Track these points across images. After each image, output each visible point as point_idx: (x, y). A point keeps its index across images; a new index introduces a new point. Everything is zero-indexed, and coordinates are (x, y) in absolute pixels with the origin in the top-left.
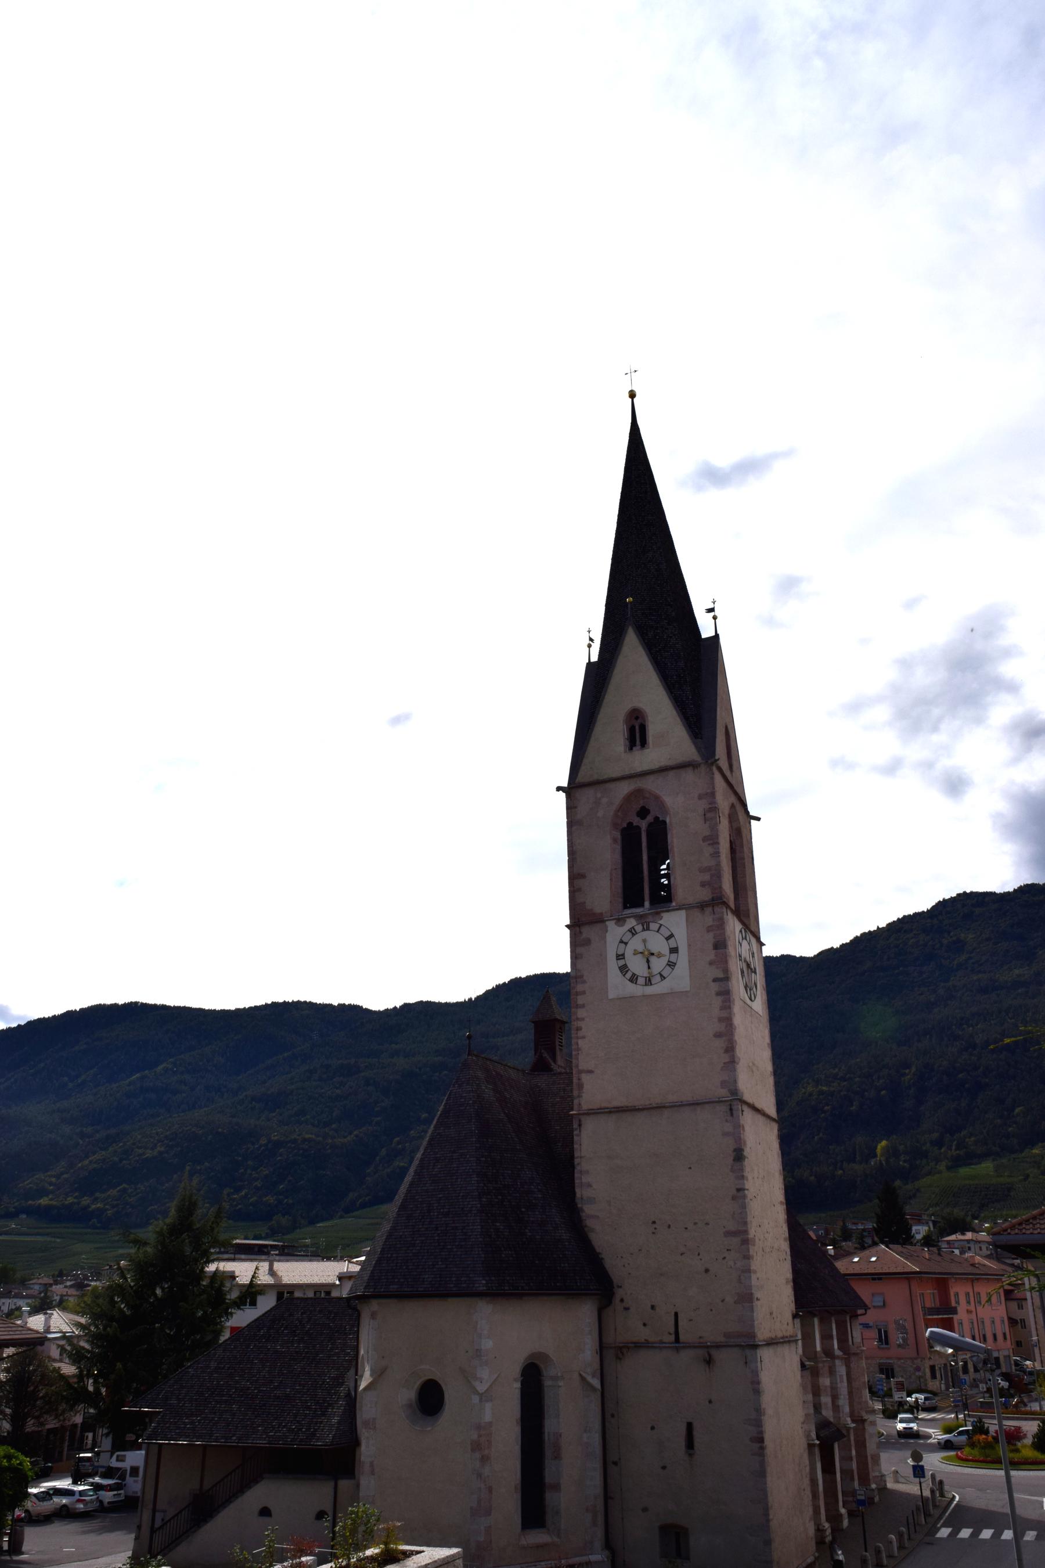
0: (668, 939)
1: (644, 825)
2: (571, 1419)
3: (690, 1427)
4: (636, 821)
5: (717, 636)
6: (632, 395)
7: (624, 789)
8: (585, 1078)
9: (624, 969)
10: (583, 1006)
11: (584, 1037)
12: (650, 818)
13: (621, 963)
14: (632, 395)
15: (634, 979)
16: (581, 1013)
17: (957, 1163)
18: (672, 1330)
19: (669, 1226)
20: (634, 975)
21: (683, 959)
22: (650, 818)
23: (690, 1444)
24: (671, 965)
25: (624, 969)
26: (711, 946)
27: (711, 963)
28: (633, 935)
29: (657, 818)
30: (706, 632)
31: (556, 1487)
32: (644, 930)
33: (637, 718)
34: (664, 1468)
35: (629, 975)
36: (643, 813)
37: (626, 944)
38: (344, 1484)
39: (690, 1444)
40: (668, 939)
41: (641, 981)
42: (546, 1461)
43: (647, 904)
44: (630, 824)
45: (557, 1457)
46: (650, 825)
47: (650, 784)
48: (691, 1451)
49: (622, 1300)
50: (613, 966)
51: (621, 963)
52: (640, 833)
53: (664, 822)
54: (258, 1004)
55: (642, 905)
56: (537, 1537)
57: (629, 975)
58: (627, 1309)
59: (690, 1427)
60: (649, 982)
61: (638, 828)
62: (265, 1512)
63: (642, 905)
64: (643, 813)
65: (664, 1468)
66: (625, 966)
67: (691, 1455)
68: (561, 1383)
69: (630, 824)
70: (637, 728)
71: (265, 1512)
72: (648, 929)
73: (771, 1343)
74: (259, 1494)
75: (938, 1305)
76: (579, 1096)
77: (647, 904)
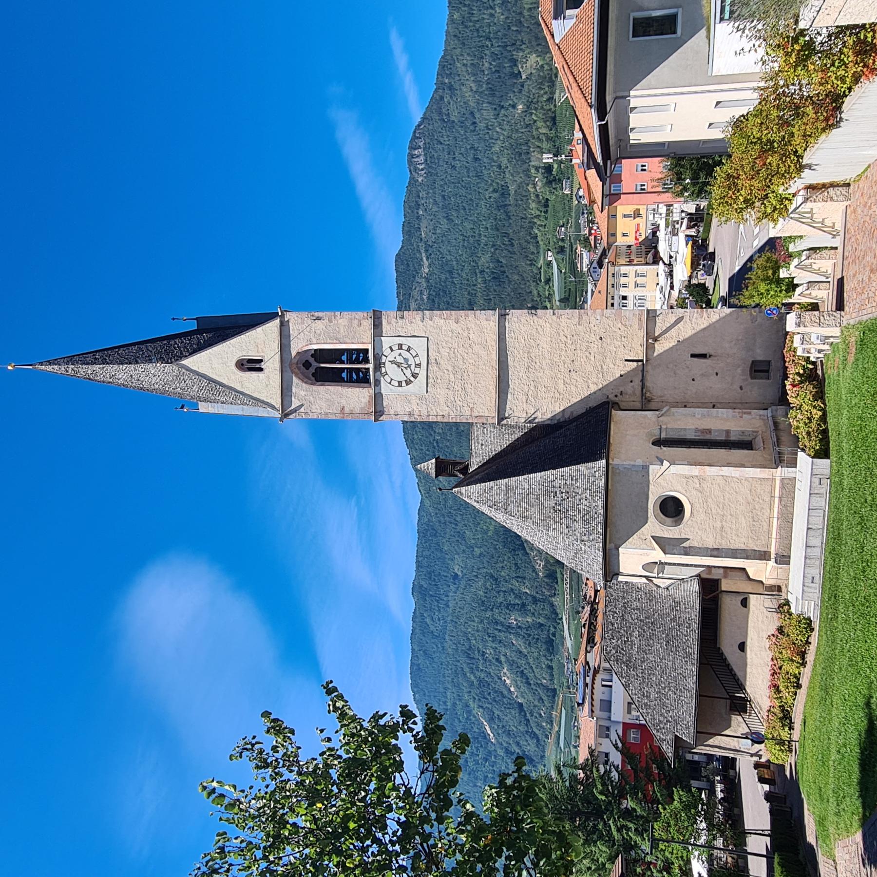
0: (392, 350)
1: (315, 364)
2: (688, 422)
3: (693, 356)
4: (312, 370)
12: (312, 360)
13: (404, 384)
17: (540, 281)
23: (703, 356)
25: (408, 382)
26: (400, 321)
29: (312, 356)
31: (728, 432)
34: (717, 374)
36: (307, 365)
38: (725, 585)
39: (703, 356)
40: (392, 350)
43: (367, 366)
44: (313, 375)
45: (709, 431)
49: (616, 396)
50: (405, 388)
51: (404, 384)
55: (368, 369)
56: (759, 442)
58: (621, 393)
59: (693, 356)
63: (368, 369)
64: (307, 365)
65: (717, 374)
67: (710, 356)
69: (313, 375)
73: (618, 722)
75: (631, 142)
77: (367, 366)
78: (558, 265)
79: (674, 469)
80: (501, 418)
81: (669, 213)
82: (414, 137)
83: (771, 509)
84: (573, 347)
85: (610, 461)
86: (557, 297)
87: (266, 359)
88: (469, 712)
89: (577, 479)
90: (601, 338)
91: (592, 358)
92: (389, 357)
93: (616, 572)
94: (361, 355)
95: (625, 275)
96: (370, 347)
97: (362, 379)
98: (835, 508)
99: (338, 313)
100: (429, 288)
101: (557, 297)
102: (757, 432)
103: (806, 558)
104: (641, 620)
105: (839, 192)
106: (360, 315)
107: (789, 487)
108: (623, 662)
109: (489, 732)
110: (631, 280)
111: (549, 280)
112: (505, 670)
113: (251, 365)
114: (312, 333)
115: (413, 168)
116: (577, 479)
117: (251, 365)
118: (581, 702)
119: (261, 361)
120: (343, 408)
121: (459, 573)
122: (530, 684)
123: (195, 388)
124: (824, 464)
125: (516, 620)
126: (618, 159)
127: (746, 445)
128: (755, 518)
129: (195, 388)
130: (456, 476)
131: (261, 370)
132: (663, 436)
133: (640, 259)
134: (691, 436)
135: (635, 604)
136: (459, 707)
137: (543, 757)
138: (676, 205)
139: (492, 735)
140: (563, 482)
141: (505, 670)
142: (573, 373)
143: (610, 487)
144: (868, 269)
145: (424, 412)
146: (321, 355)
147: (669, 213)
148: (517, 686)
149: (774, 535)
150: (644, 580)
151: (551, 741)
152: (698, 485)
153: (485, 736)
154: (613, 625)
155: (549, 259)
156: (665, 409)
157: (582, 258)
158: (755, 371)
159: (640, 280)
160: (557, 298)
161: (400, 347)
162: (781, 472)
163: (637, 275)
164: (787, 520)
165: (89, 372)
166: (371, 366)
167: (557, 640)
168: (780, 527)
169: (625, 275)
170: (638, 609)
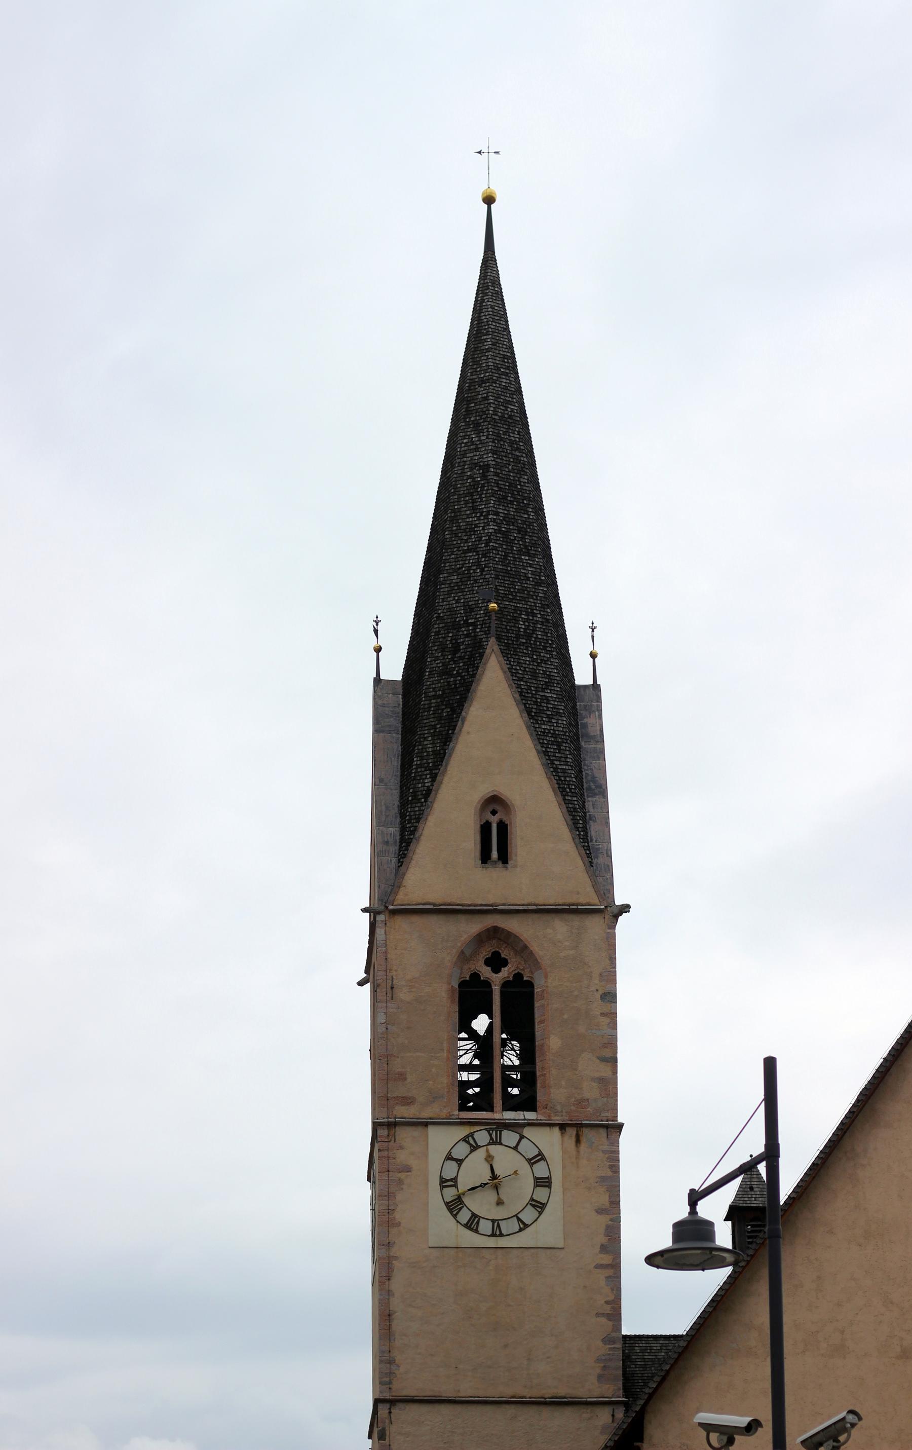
0: (532, 1162)
1: (497, 980)
3: (770, 1065)
4: (486, 972)
5: (596, 687)
6: (489, 200)
7: (473, 927)
12: (505, 973)
14: (489, 200)
15: (472, 1224)
21: (556, 1199)
22: (505, 973)
29: (518, 976)
30: (582, 677)
32: (492, 1142)
33: (496, 962)
35: (464, 1216)
37: (460, 1162)
44: (475, 976)
46: (505, 985)
47: (512, 925)
50: (436, 1200)
52: (491, 993)
53: (530, 985)
57: (464, 1216)
59: (770, 1065)
61: (487, 984)
70: (495, 854)
113: (495, 841)
117: (495, 841)
119: (504, 857)
131: (485, 857)
161: (543, 1182)
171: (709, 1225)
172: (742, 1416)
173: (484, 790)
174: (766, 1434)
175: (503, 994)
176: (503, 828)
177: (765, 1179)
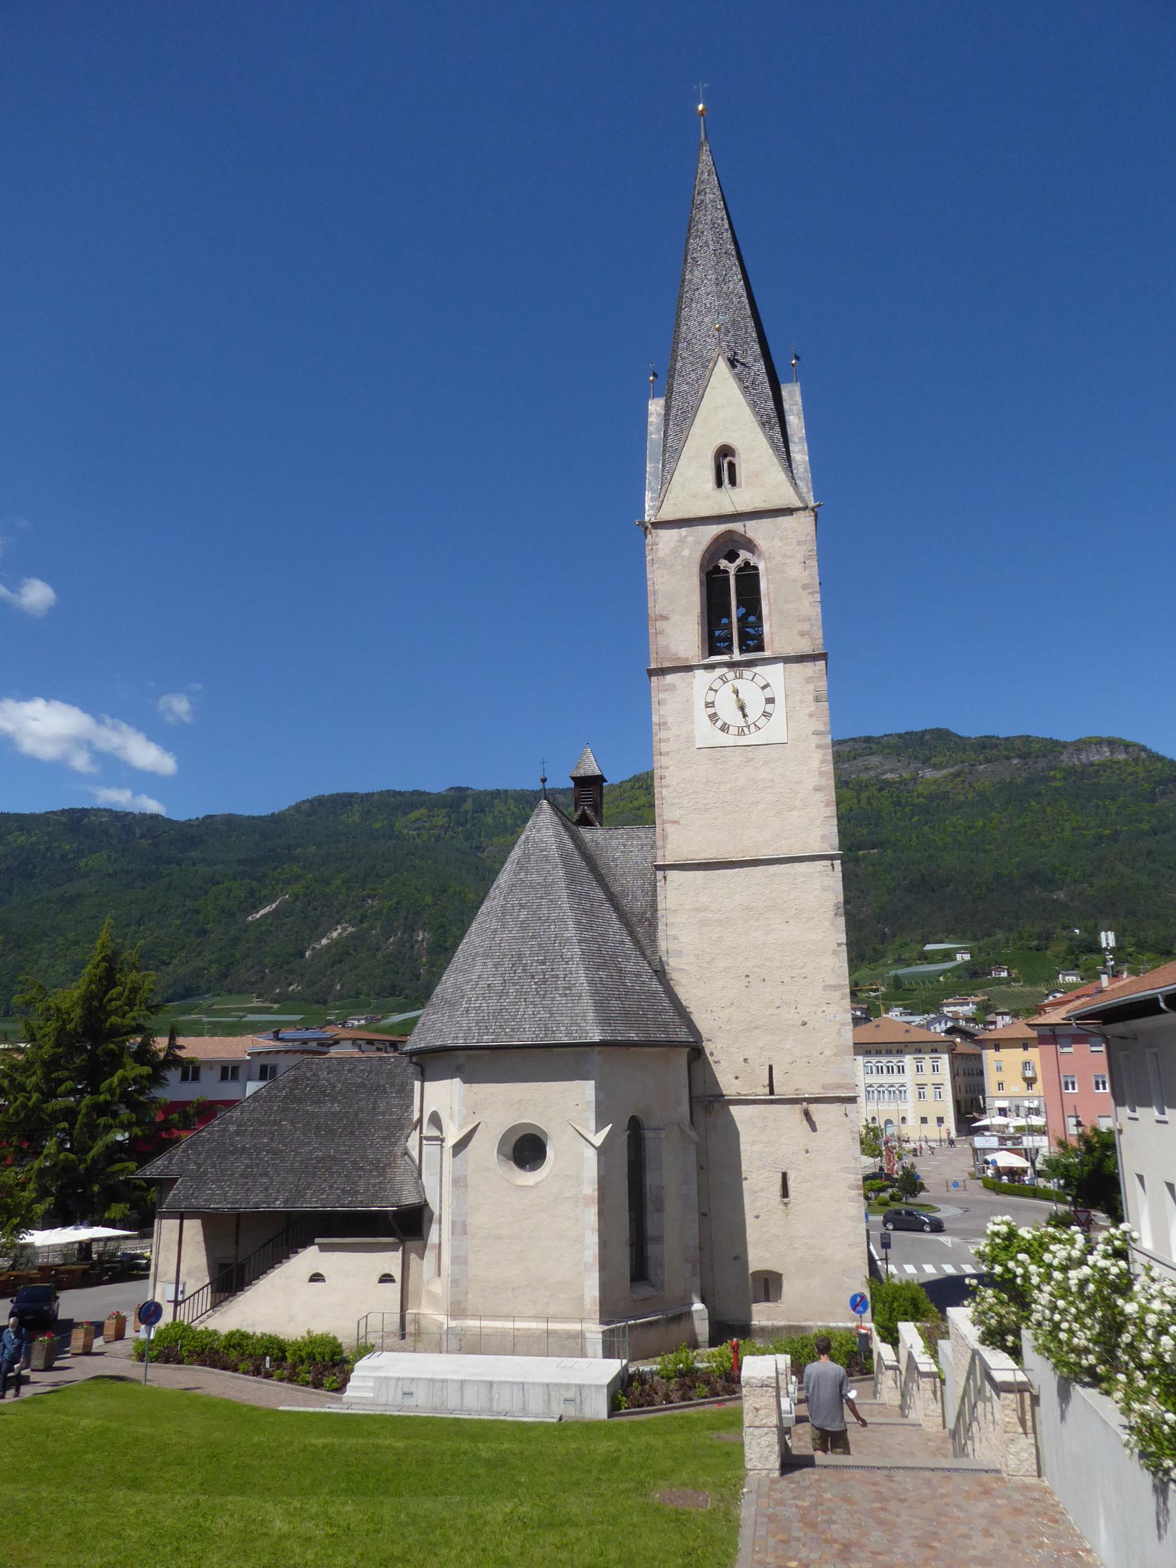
0: (764, 688)
1: (732, 568)
7: (715, 530)
8: (669, 828)
9: (714, 717)
10: (667, 754)
11: (668, 786)
12: (739, 562)
13: (711, 711)
15: (724, 728)
16: (665, 761)
18: (767, 1082)
19: (764, 980)
20: (725, 724)
21: (779, 709)
22: (739, 562)
23: (785, 1193)
24: (767, 715)
25: (714, 717)
26: (811, 698)
27: (811, 716)
28: (725, 682)
29: (747, 564)
31: (659, 1239)
32: (736, 678)
33: (725, 456)
35: (719, 724)
37: (716, 691)
39: (785, 1193)
40: (764, 688)
41: (733, 730)
42: (648, 1215)
43: (736, 650)
45: (660, 1209)
46: (740, 569)
47: (737, 527)
48: (786, 1200)
50: (701, 714)
51: (711, 711)
54: (37, 812)
55: (729, 650)
56: (644, 1291)
57: (719, 724)
60: (741, 732)
62: (757, 1217)
66: (715, 714)
67: (786, 1204)
68: (663, 1134)
71: (316, 1278)
72: (741, 677)
74: (309, 1259)
76: (664, 847)
77: (736, 650)
78: (949, 971)
79: (591, 1156)
80: (660, 868)
81: (1033, 1130)
82: (1127, 746)
83: (536, 1318)
84: (787, 979)
85: (597, 1049)
86: (902, 971)
87: (737, 490)
88: (288, 882)
89: (566, 995)
90: (804, 1024)
91: (771, 1011)
92: (749, 685)
93: (427, 1072)
94: (752, 640)
95: (935, 1069)
96: (767, 654)
97: (715, 642)
98: (522, 1430)
99: (818, 597)
100: (903, 782)
101: (902, 971)
102: (662, 1288)
103: (444, 1381)
104: (357, 1115)
105: (1025, 1455)
106: (818, 633)
107: (574, 1346)
108: (292, 1090)
109: (262, 912)
110: (928, 1077)
111: (926, 959)
112: (350, 929)
113: (725, 465)
114: (786, 560)
115: (1081, 745)
116: (566, 995)
117: (725, 465)
118: (281, 1036)
119: (733, 482)
120: (666, 618)
121: (485, 854)
122: (333, 965)
123: (685, 388)
124: (598, 1408)
125: (423, 940)
126: (1105, 1036)
127: (640, 1270)
128: (485, 1295)
129: (685, 388)
130: (576, 810)
131: (719, 483)
132: (648, 1134)
133: (963, 1089)
134: (651, 1179)
135: (382, 1105)
136: (296, 868)
137: (230, 991)
138: (1045, 1139)
139: (258, 916)
140: (561, 974)
141: (350, 929)
142: (745, 981)
143: (555, 1050)
144: (853, 1535)
145: (664, 747)
146: (749, 578)
147: (1033, 1130)
148: (328, 947)
149: (485, 1323)
150: (416, 1116)
151: (256, 1003)
152: (567, 1195)
153: (255, 908)
154: (350, 1071)
155: (959, 957)
156: (693, 1134)
157: (962, 1005)
158: (766, 1280)
159: (929, 1091)
160: (900, 972)
161: (771, 701)
162: (594, 1331)
163: (937, 1086)
164: (512, 1345)
165: (700, 227)
166: (737, 656)
167: (393, 1001)
168: (503, 1334)
169: (935, 1069)
170: (374, 1108)
171: (738, 556)
172: (289, 1412)
173: (719, 442)
174: (813, 1108)
175: (737, 576)
176: (732, 466)
177: (706, 158)
